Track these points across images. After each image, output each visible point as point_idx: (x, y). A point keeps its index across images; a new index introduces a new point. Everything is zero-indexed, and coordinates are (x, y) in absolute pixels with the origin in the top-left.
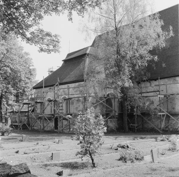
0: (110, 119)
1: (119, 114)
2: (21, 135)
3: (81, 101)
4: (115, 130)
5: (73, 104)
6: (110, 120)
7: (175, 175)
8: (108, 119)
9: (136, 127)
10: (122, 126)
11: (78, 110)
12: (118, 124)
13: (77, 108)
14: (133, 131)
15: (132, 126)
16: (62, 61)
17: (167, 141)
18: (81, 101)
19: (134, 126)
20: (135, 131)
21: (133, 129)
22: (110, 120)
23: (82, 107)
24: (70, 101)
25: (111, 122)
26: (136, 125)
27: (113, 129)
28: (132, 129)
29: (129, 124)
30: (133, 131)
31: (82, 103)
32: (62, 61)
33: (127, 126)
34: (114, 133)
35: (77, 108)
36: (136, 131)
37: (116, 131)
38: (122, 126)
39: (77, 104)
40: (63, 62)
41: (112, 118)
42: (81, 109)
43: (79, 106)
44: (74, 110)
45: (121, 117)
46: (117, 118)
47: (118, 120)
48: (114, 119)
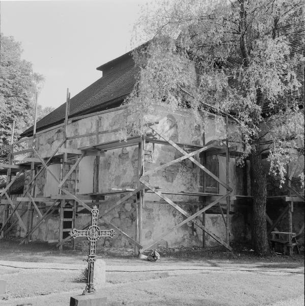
0: (212, 215)
1: (239, 201)
2: (280, 263)
3: (130, 156)
4: (227, 246)
5: (108, 169)
6: (212, 218)
7: (298, 304)
8: (207, 215)
9: (294, 241)
10: (243, 235)
11: (121, 183)
12: (235, 230)
13: (118, 178)
14: (282, 252)
15: (277, 235)
16: (99, 69)
17: (62, 219)
18: (130, 156)
19: (286, 236)
20: (288, 254)
21: (283, 244)
22: (212, 218)
23: (133, 174)
24: (102, 159)
25: (214, 223)
26: (292, 234)
27: (222, 242)
28: (279, 243)
29: (270, 228)
30: (282, 252)
31: (133, 162)
32: (99, 69)
33: (266, 237)
34: (225, 255)
35: (118, 178)
36: (291, 252)
37: (231, 249)
38: (243, 235)
39: (119, 165)
40: (101, 72)
41: (220, 213)
42: (130, 181)
43: (125, 172)
44: (110, 185)
45: (243, 211)
46: (231, 213)
47: (234, 220)
48: (225, 216)
